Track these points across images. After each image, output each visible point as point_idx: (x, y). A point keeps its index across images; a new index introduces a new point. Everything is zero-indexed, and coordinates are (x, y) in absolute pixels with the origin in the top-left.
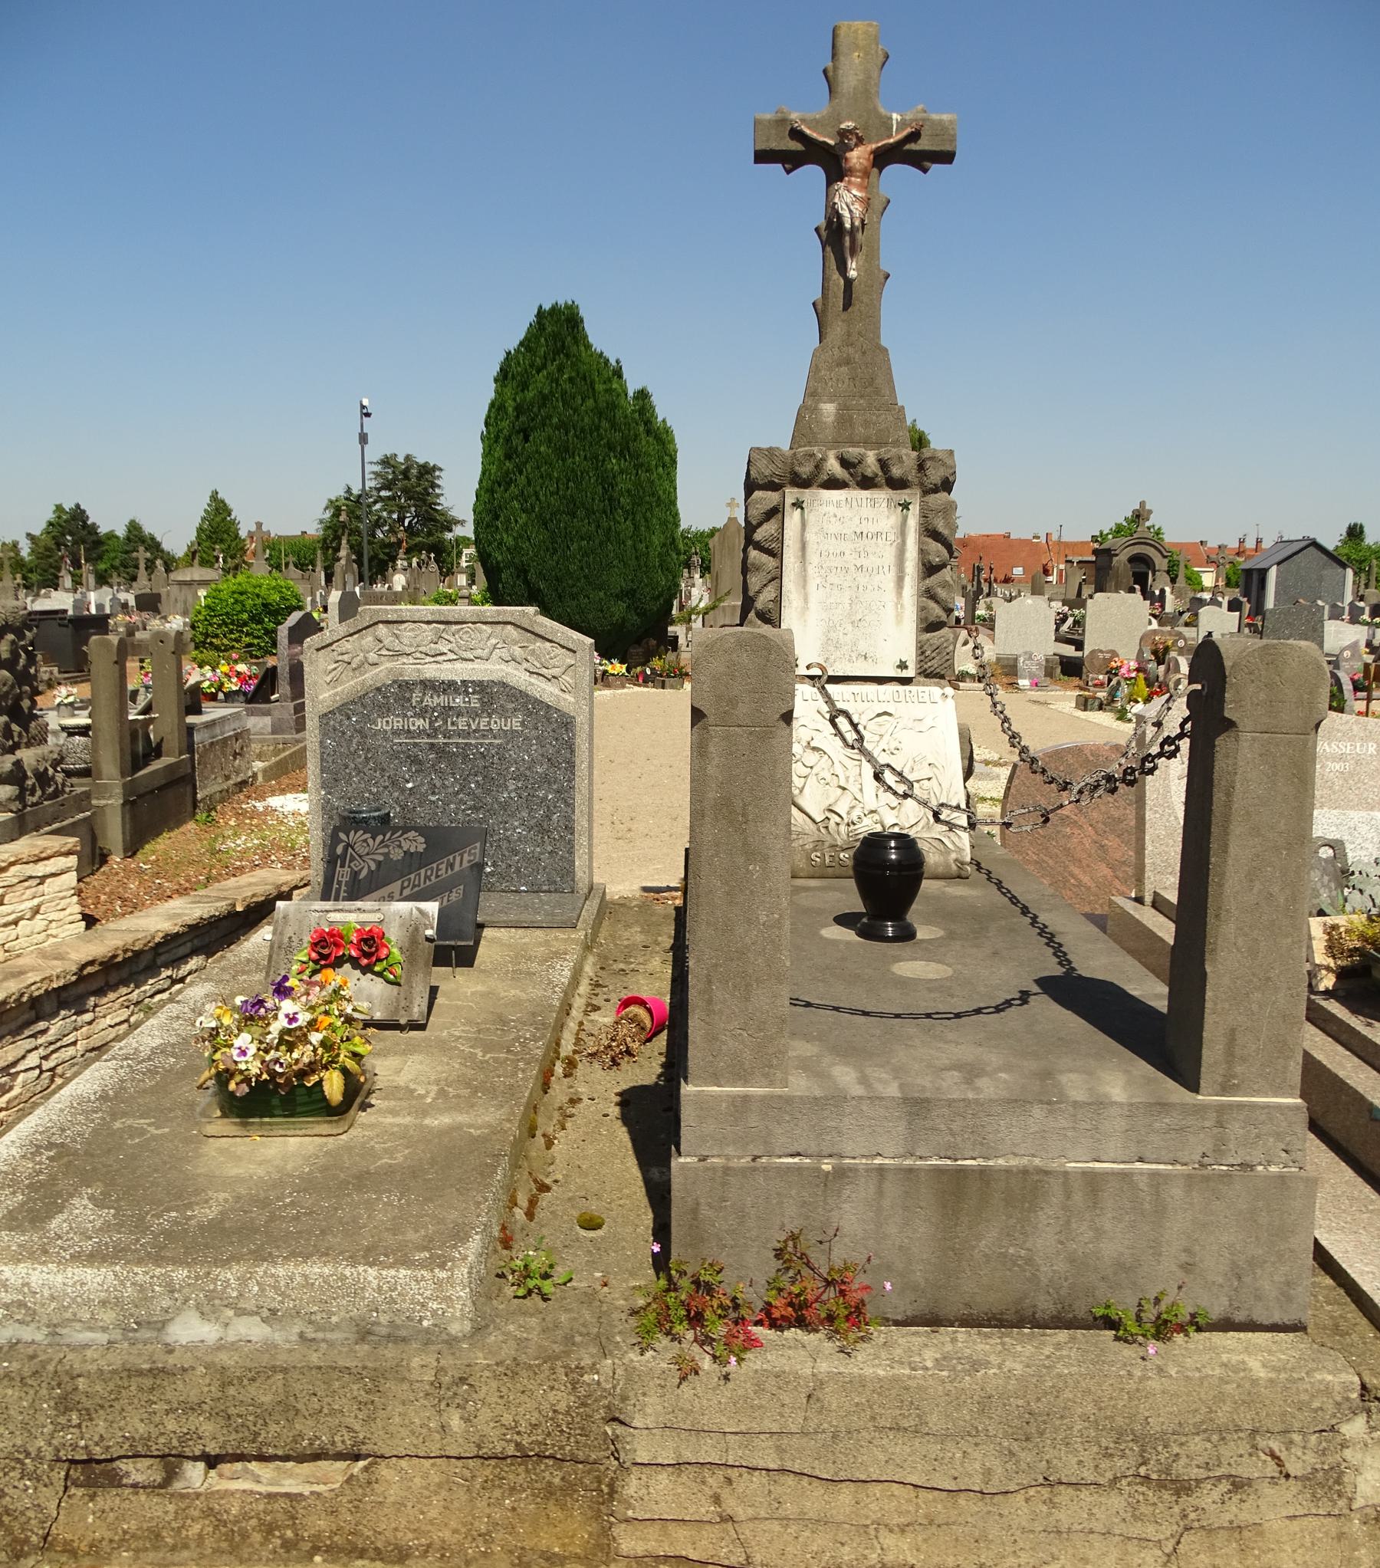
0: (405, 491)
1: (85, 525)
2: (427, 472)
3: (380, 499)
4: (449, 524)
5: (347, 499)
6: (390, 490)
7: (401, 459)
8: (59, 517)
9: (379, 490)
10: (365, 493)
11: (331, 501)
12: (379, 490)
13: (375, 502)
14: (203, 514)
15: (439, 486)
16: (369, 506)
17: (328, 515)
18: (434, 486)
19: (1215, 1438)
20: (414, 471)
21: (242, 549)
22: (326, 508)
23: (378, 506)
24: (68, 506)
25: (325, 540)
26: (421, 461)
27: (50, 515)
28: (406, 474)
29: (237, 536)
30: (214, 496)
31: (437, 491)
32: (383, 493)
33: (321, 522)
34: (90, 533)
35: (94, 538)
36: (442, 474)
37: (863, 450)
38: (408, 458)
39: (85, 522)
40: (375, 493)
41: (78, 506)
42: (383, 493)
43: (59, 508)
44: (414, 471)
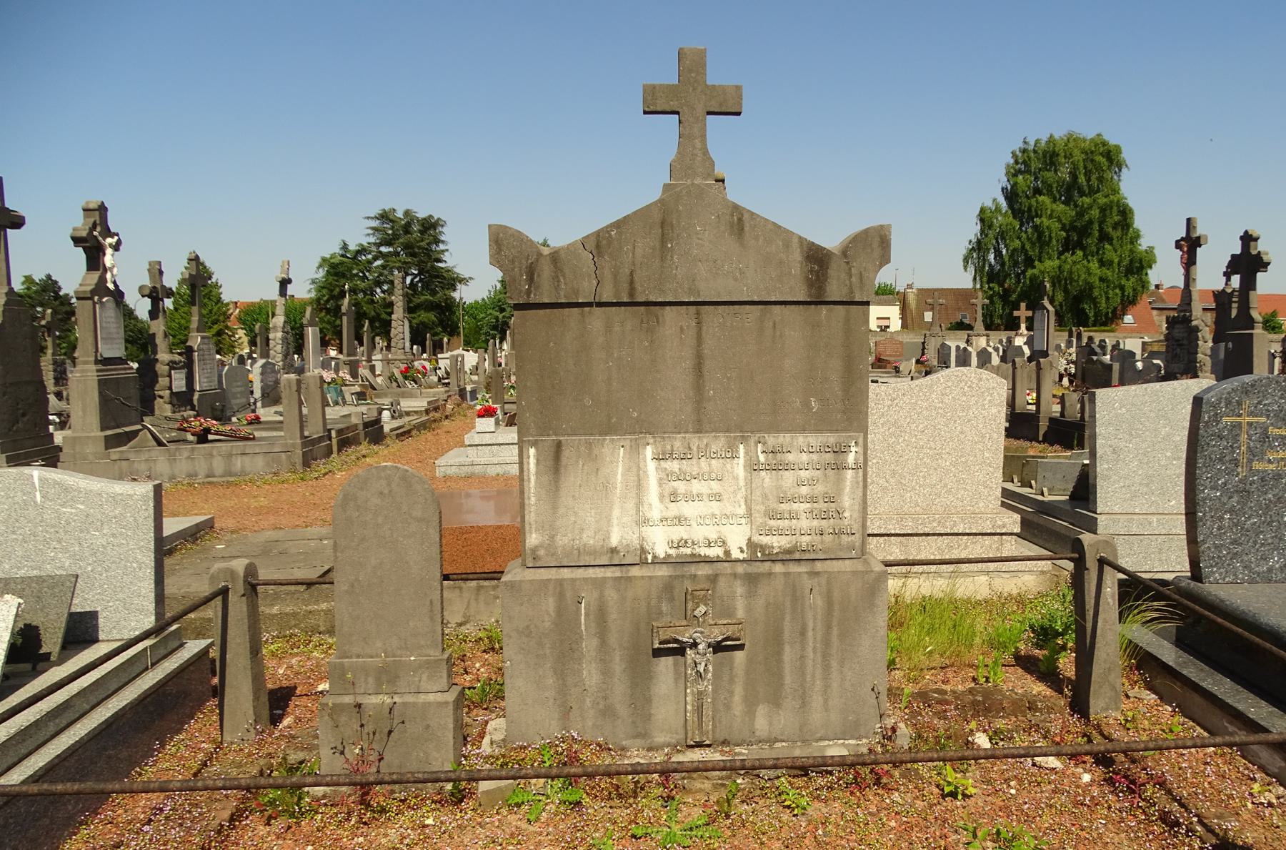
0: (407, 247)
1: (57, 297)
2: (430, 226)
3: (381, 255)
4: (452, 281)
5: (342, 256)
6: (988, 250)
7: (400, 214)
8: (28, 289)
9: (379, 245)
10: (362, 251)
11: (324, 260)
12: (381, 244)
13: (375, 259)
14: (180, 277)
15: (443, 242)
16: (370, 262)
17: (321, 274)
18: (437, 242)
19: (1058, 739)
20: (416, 228)
21: (225, 313)
22: (320, 266)
23: (379, 263)
24: (38, 276)
25: (318, 300)
26: (422, 215)
28: (407, 229)
29: (219, 300)
30: (195, 260)
31: (442, 247)
32: (384, 249)
33: (313, 282)
34: (62, 304)
35: (68, 309)
36: (444, 229)
37: (233, 323)
38: (407, 213)
39: (57, 293)
40: (374, 248)
41: (49, 277)
42: (384, 249)
44: (416, 228)
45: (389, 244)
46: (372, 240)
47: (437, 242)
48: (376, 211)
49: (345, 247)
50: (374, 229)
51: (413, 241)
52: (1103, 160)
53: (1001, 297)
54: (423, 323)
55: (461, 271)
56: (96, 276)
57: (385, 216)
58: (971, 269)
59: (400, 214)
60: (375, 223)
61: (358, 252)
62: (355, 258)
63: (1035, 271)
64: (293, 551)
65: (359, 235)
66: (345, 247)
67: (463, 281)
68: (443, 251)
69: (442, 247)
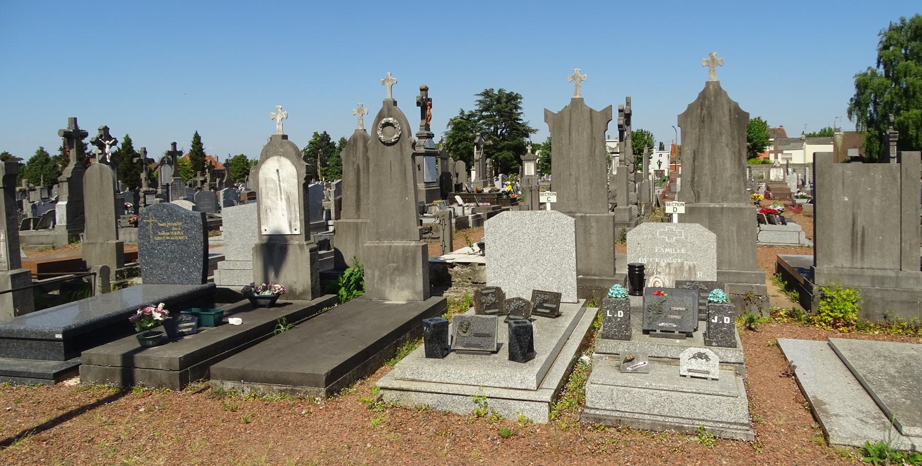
1: (328, 144)
4: (526, 132)
7: (496, 92)
9: (482, 111)
10: (472, 115)
12: (482, 111)
13: (479, 120)
16: (475, 122)
17: (450, 129)
18: (517, 107)
24: (320, 133)
27: (311, 138)
28: (499, 101)
31: (519, 111)
32: (484, 113)
38: (500, 91)
40: (479, 113)
41: (325, 133)
42: (484, 113)
43: (316, 134)
45: (486, 110)
46: (477, 108)
47: (517, 107)
48: (482, 91)
49: (462, 112)
50: (480, 101)
51: (502, 107)
52: (513, 99)
53: (877, 138)
54: (505, 158)
55: (532, 125)
56: (424, 121)
57: (487, 94)
58: (855, 118)
59: (496, 92)
60: (481, 98)
61: (469, 115)
62: (468, 119)
63: (902, 118)
64: (34, 240)
65: (471, 105)
66: (462, 112)
67: (534, 131)
68: (519, 114)
69: (519, 111)
